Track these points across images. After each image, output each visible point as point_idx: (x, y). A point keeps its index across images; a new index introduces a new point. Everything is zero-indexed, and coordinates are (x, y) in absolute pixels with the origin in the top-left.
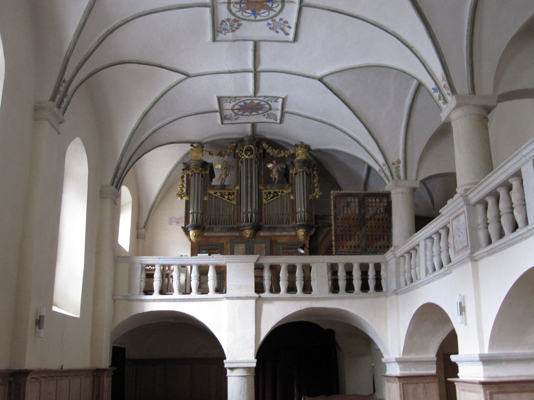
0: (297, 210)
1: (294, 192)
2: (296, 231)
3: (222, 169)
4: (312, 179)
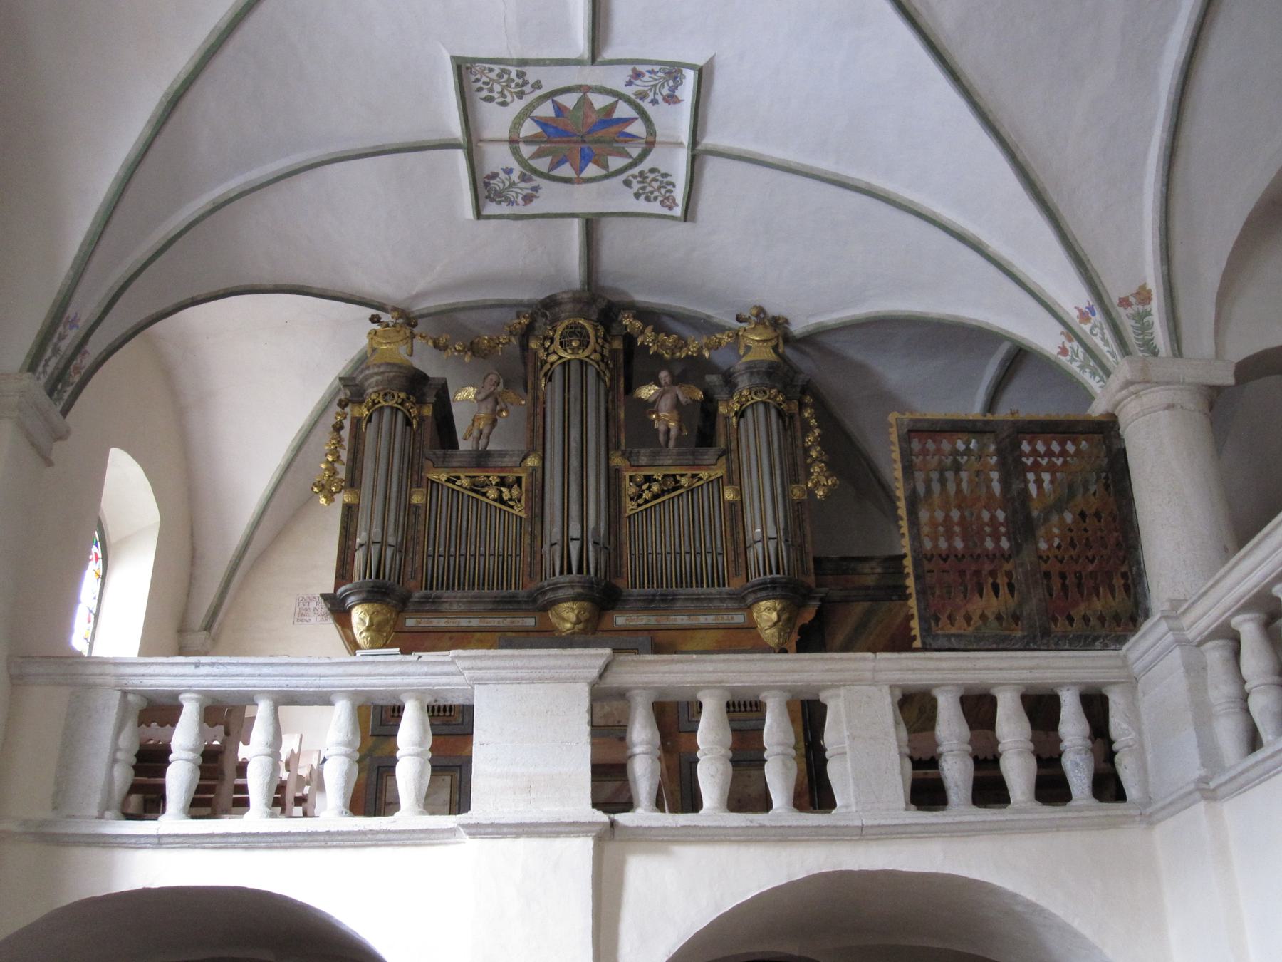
0: (749, 535)
1: (735, 478)
2: (749, 607)
4: (799, 434)
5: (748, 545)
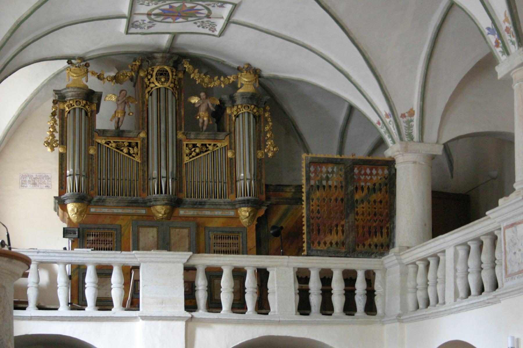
0: (238, 176)
1: (233, 146)
2: (237, 209)
3: (119, 102)
4: (262, 125)
5: (237, 180)
